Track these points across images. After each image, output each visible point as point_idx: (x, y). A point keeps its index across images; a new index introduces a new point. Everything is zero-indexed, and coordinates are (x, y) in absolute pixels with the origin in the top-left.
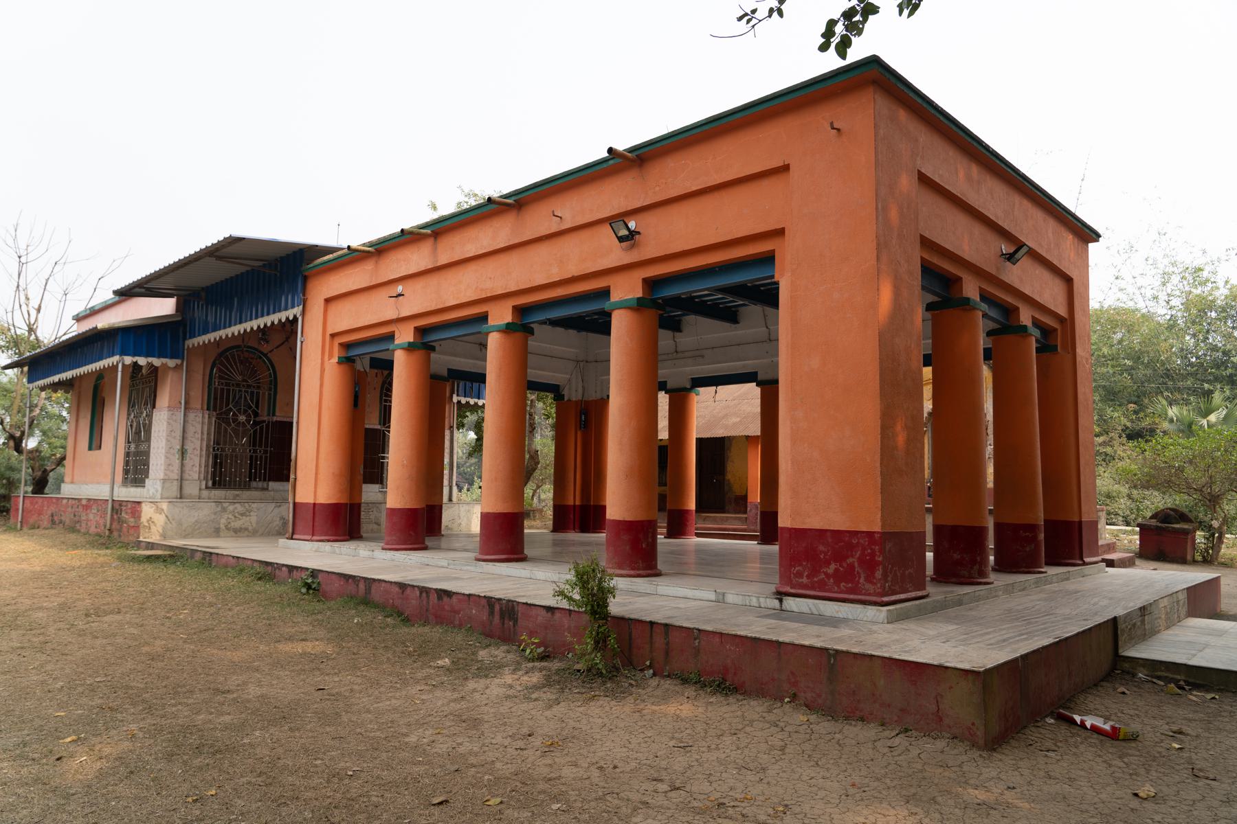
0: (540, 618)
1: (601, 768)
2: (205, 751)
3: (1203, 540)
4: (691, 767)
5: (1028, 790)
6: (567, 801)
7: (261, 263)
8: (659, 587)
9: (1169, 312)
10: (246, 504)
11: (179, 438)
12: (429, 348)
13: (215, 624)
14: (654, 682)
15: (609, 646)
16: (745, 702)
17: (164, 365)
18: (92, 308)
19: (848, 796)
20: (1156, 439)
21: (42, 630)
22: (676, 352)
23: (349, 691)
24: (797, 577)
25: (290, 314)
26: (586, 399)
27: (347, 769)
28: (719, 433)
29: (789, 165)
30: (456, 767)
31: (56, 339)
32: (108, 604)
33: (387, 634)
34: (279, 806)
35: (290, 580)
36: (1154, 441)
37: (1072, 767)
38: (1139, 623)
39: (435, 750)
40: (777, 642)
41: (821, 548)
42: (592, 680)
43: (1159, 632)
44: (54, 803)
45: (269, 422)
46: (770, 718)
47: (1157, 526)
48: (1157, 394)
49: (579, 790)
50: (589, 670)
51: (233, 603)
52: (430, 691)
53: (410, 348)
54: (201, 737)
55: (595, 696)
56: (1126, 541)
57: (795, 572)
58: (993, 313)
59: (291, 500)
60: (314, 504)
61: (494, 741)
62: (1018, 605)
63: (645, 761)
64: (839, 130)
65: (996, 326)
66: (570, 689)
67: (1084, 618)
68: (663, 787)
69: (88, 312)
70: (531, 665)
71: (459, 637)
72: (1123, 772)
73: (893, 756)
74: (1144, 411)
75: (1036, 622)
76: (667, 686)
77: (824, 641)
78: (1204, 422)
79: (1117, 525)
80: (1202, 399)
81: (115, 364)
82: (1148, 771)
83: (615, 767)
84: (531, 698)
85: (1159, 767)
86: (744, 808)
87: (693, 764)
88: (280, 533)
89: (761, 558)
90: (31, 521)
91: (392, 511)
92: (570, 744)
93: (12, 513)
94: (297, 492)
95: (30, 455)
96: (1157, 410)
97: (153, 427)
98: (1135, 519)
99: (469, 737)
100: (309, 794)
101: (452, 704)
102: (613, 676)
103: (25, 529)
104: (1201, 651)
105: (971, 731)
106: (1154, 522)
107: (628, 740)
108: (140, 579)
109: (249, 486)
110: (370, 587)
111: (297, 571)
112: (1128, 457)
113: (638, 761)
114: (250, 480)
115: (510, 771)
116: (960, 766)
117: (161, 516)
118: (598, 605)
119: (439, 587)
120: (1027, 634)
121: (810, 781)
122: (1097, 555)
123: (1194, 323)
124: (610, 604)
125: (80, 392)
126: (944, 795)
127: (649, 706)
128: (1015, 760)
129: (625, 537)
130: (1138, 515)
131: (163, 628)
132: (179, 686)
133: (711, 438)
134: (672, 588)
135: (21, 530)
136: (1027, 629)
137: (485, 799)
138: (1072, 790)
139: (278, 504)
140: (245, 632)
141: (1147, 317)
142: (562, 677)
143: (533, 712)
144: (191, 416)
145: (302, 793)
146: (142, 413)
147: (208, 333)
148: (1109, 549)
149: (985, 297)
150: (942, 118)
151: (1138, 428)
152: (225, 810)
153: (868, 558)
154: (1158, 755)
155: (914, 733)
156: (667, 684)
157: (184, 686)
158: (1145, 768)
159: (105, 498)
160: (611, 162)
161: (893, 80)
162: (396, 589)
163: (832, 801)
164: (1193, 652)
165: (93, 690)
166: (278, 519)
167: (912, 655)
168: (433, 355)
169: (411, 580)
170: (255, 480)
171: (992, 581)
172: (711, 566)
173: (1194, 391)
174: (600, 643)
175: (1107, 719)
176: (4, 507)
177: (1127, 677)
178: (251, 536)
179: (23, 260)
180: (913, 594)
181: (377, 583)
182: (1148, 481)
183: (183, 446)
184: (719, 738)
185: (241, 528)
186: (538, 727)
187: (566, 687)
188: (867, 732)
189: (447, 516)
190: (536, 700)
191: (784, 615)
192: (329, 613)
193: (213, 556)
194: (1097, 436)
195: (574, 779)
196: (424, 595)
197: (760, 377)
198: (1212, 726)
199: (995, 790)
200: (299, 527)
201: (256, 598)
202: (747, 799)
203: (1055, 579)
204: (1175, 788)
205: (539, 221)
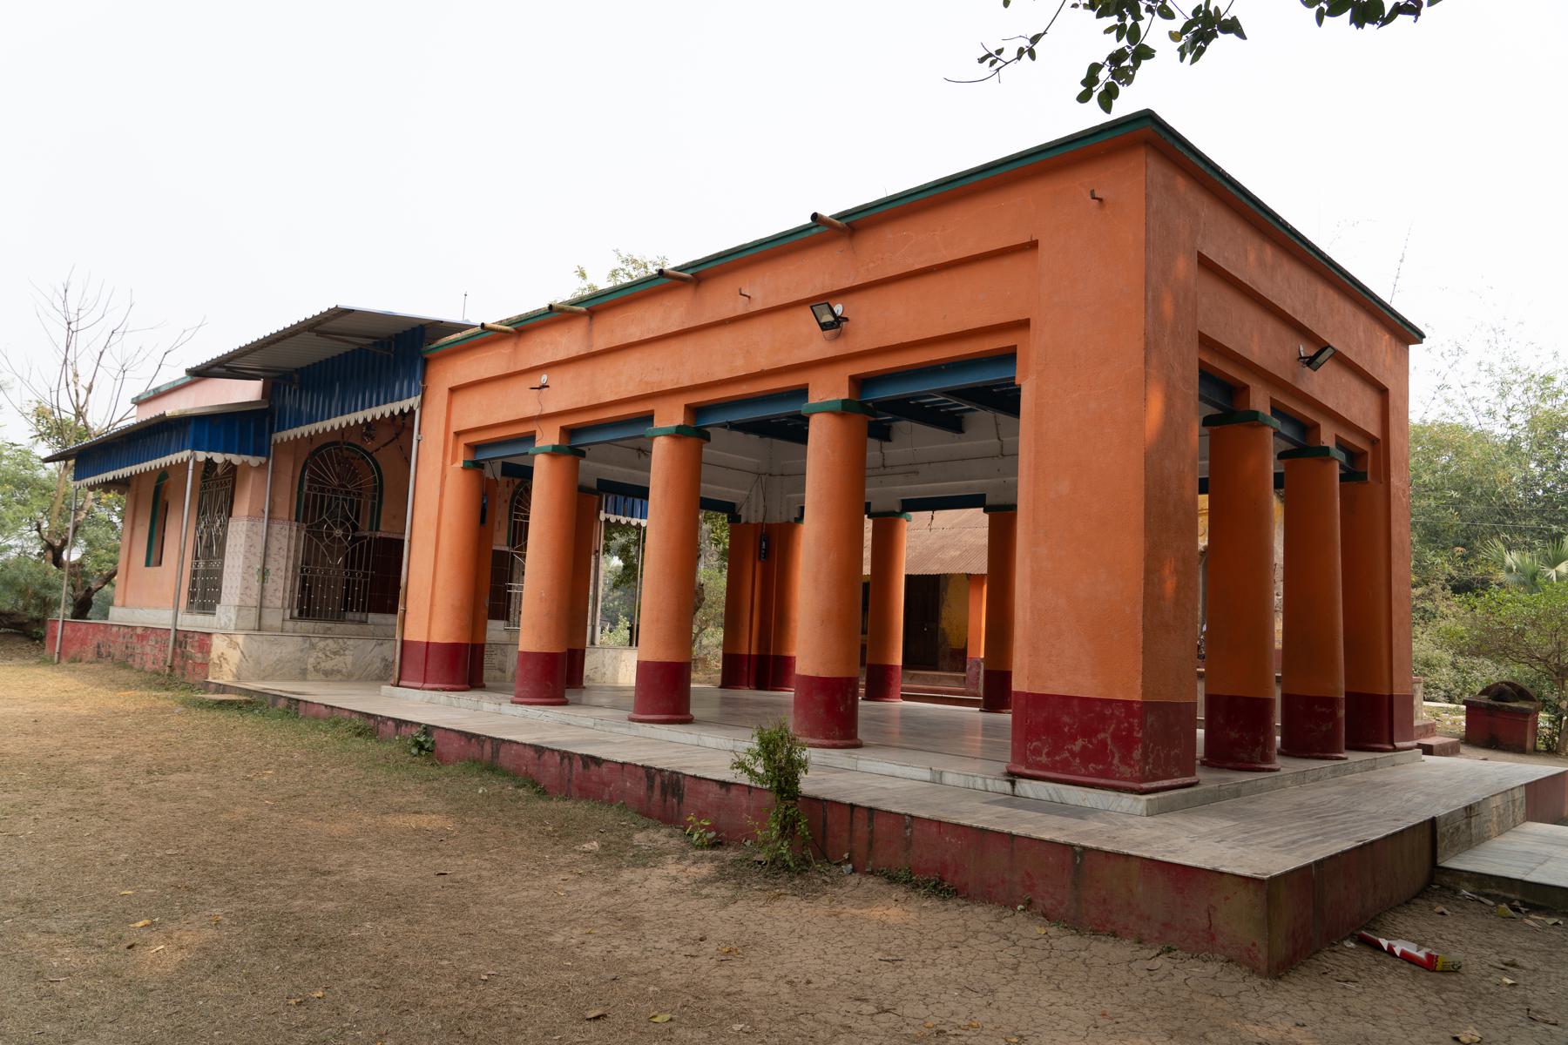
0: (711, 796)
1: (791, 983)
2: (306, 944)
3: (1547, 725)
4: (901, 985)
5: (1321, 1029)
6: (752, 1022)
7: (370, 341)
8: (860, 762)
9: (1510, 432)
10: (340, 641)
11: (259, 555)
12: (578, 453)
13: (306, 788)
14: (854, 879)
15: (799, 833)
16: (967, 908)
17: (245, 464)
18: (157, 389)
19: (1097, 1027)
20: (1489, 594)
21: (96, 789)
22: (884, 466)
23: (477, 877)
24: (1034, 755)
25: (405, 405)
26: (768, 522)
27: (479, 972)
28: (933, 569)
29: (1037, 241)
30: (614, 975)
31: (109, 426)
32: (174, 759)
33: (519, 809)
34: (400, 1013)
35: (397, 738)
36: (1487, 596)
37: (1377, 1002)
38: (1464, 827)
39: (586, 954)
40: (1010, 835)
41: (1066, 719)
42: (776, 874)
43: (1489, 838)
44: (130, 999)
45: (371, 538)
46: (999, 929)
47: (1489, 705)
48: (1492, 535)
49: (765, 1009)
50: (773, 862)
51: (327, 764)
52: (576, 881)
53: (554, 452)
54: (300, 928)
55: (781, 894)
56: (1448, 723)
57: (1031, 748)
58: (1287, 431)
59: (398, 637)
60: (428, 643)
61: (658, 945)
62: (1311, 799)
63: (845, 977)
64: (1101, 200)
65: (1290, 447)
66: (749, 885)
67: (1394, 818)
68: (868, 1008)
69: (152, 394)
70: (699, 853)
71: (609, 816)
72: (1441, 1010)
73: (1152, 981)
74: (1474, 557)
75: (1334, 821)
76: (869, 885)
77: (1067, 836)
78: (1552, 573)
79: (1437, 701)
80: (1550, 543)
81: (185, 460)
82: (1472, 1011)
83: (809, 982)
84: (701, 894)
85: (1485, 1007)
86: (970, 1037)
87: (904, 982)
88: (382, 678)
89: (984, 729)
90: (71, 653)
91: (526, 656)
92: (752, 952)
93: (47, 642)
94: (406, 627)
95: (71, 570)
96: (1491, 556)
97: (228, 540)
98: (1461, 694)
99: (627, 939)
100: (434, 1001)
101: (604, 898)
102: (803, 870)
103: (63, 661)
104: (1541, 864)
105: (1251, 954)
106: (1484, 699)
107: (823, 950)
108: (211, 730)
109: (344, 617)
110: (498, 751)
111: (406, 725)
112: (1454, 615)
113: (836, 976)
114: (346, 610)
115: (680, 982)
116: (1237, 996)
117: (235, 652)
118: (787, 781)
119: (585, 753)
120: (1322, 834)
121: (1049, 1008)
122: (1411, 739)
123: (1540, 446)
124: (801, 781)
125: (137, 495)
126: (1217, 1031)
127: (848, 909)
128: (1305, 991)
129: (819, 698)
130: (1464, 689)
131: (243, 792)
132: (269, 864)
133: (922, 575)
134: (875, 763)
135: (58, 663)
136: (1322, 829)
137: (651, 1015)
138: (1375, 1030)
139: (380, 642)
140: (345, 800)
141: (1481, 437)
142: (739, 869)
143: (704, 912)
144: (276, 527)
145: (428, 999)
146: (214, 522)
147: (301, 425)
148: (1427, 732)
149: (1277, 410)
150: (1229, 188)
151: (1466, 578)
152: (335, 1016)
153: (1124, 733)
154: (1485, 992)
155: (1180, 954)
156: (870, 882)
157: (275, 864)
158: (1468, 1008)
159: (167, 628)
160: (815, 231)
161: (1170, 140)
162: (531, 754)
163: (1079, 1033)
164: (1532, 865)
165: (164, 865)
166: (379, 660)
167: (1178, 857)
168: (582, 462)
169: (550, 743)
170: (351, 610)
171: (1278, 767)
172: (920, 737)
173: (1540, 533)
174: (788, 828)
175: (1421, 945)
176: (37, 633)
177: (1447, 893)
178: (344, 681)
179: (73, 327)
180: (1180, 781)
181: (507, 746)
182: (1478, 647)
183: (264, 565)
184: (935, 952)
185: (333, 670)
186: (711, 930)
187: (745, 881)
188: (1121, 951)
189: (590, 661)
190: (707, 896)
191: (1017, 801)
192: (447, 780)
193: (301, 703)
194: (1414, 586)
195: (758, 995)
196: (566, 761)
197: (988, 502)
198: (1553, 958)
199: (1280, 1027)
200: (408, 671)
201: (355, 759)
202: (972, 1026)
203: (1357, 768)
204: (1505, 1033)
205: (722, 300)
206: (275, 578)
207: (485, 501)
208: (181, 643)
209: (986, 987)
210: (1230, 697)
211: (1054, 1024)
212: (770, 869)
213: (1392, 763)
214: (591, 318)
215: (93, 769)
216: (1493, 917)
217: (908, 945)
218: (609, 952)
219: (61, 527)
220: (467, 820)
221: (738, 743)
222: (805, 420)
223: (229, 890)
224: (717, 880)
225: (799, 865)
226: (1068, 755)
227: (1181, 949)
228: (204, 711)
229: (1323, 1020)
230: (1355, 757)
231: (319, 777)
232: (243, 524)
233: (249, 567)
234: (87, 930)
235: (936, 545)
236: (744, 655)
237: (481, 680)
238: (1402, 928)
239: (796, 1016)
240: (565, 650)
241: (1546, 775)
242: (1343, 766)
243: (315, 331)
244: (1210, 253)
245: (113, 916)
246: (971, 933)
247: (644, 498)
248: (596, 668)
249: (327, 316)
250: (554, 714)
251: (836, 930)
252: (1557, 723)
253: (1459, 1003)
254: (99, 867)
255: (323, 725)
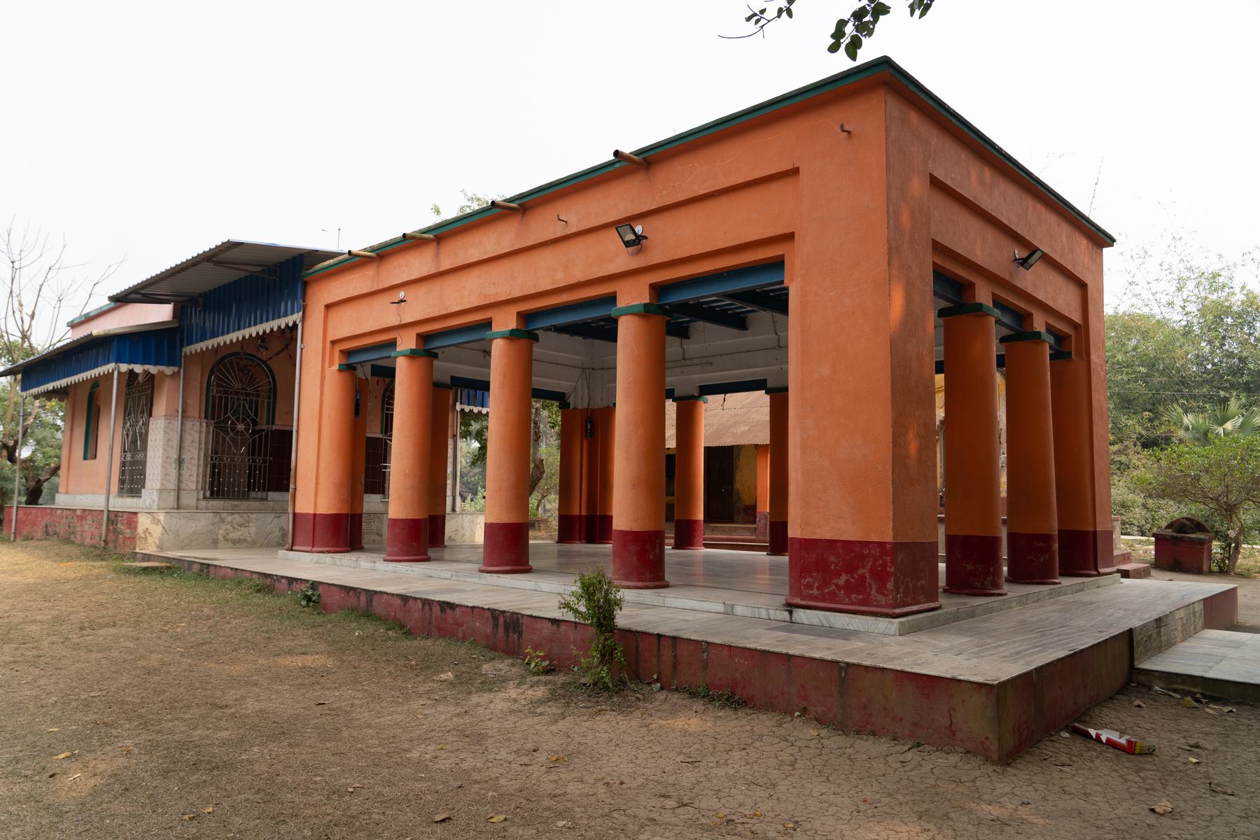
0: (545, 631)
1: (607, 784)
2: (202, 768)
3: (1219, 551)
4: (699, 782)
5: (1043, 806)
6: (573, 819)
7: (260, 269)
9: (1185, 318)
10: (245, 515)
12: (432, 355)
14: (662, 696)
15: (616, 659)
16: (754, 716)
18: (87, 314)
21: (35, 644)
22: (684, 359)
25: (290, 320)
27: (347, 785)
28: (728, 441)
29: (798, 168)
30: (459, 783)
34: (277, 823)
35: (289, 593)
36: (1169, 449)
37: (1087, 782)
38: (1155, 635)
40: (787, 655)
41: (832, 559)
42: (598, 694)
43: (1175, 644)
45: (268, 431)
48: (1172, 401)
50: (595, 684)
51: (231, 616)
52: (433, 706)
53: (412, 355)
56: (1141, 552)
57: (805, 583)
58: (1006, 319)
59: (290, 510)
60: (315, 515)
61: (498, 757)
62: (1032, 617)
63: (652, 777)
64: (849, 132)
66: (575, 703)
68: (671, 803)
69: (83, 318)
70: (535, 679)
71: (462, 651)
72: (1140, 787)
74: (1159, 419)
75: (1051, 634)
76: (675, 700)
77: (834, 654)
78: (1220, 430)
79: (1131, 535)
81: (110, 371)
82: (1164, 786)
83: (622, 783)
86: (754, 825)
87: (701, 780)
89: (770, 569)
90: (25, 532)
95: (23, 465)
96: (1172, 418)
98: (1151, 529)
99: (473, 753)
100: (309, 812)
101: (455, 719)
102: (620, 690)
103: (18, 540)
104: (1218, 663)
106: (1169, 532)
107: (635, 755)
109: (248, 496)
110: (371, 600)
111: (297, 583)
112: (1143, 465)
113: (645, 777)
114: (249, 490)
117: (158, 527)
118: (605, 617)
119: (442, 599)
120: (1041, 646)
121: (820, 797)
124: (617, 617)
128: (1029, 775)
129: (633, 548)
131: (159, 642)
132: (176, 701)
135: (14, 541)
136: (1041, 641)
139: (278, 515)
140: (244, 645)
141: (1162, 324)
143: (538, 727)
144: (189, 424)
146: (138, 422)
147: (206, 340)
149: (998, 303)
151: (1153, 436)
152: (222, 828)
154: (1174, 770)
155: (927, 748)
156: (675, 698)
160: (618, 165)
161: (904, 81)
162: (398, 602)
163: (844, 817)
165: (87, 706)
166: (278, 530)
168: (436, 363)
169: (413, 592)
170: (254, 490)
172: (719, 577)
173: (1210, 399)
174: (607, 655)
175: (1122, 733)
177: (1143, 690)
178: (249, 547)
179: (17, 265)
180: (925, 606)
181: (379, 596)
182: (1163, 490)
183: (180, 455)
184: (727, 754)
185: (240, 539)
187: (572, 701)
188: (881, 746)
189: (450, 527)
190: (541, 714)
191: (795, 627)
192: (329, 626)
193: (211, 568)
194: (1112, 444)
195: (580, 795)
197: (769, 385)
198: (1229, 739)
199: (1009, 806)
200: (299, 539)
202: (756, 815)
203: (1069, 590)
204: (1192, 804)
205: (544, 225)
206: (189, 466)
207: (358, 397)
208: (113, 521)
209: (769, 781)
210: (965, 537)
211: (824, 811)
212: (592, 690)
213: (1097, 586)
214: (438, 243)
215: (34, 627)
216: (1179, 707)
217: (705, 749)
218: (457, 764)
219: (13, 430)
220: (344, 658)
221: (568, 587)
222: (615, 321)
223: (141, 724)
224: (549, 700)
225: (616, 686)
226: (834, 588)
227: (929, 744)
228: (132, 576)
229: (1044, 799)
230: (1066, 582)
231: (223, 627)
232: (161, 423)
233: (167, 457)
234: (17, 763)
235: (728, 423)
236: (575, 516)
237: (360, 543)
238: (1107, 720)
239: (611, 812)
240: (427, 516)
241: (1219, 591)
242: (1057, 590)
243: (213, 262)
244: (940, 174)
245: (40, 750)
246: (757, 737)
247: (486, 390)
248: (457, 530)
249: (221, 249)
250: (418, 569)
251: (646, 738)
252: (1227, 549)
253: (1154, 780)
254: (31, 709)
255: (230, 584)
